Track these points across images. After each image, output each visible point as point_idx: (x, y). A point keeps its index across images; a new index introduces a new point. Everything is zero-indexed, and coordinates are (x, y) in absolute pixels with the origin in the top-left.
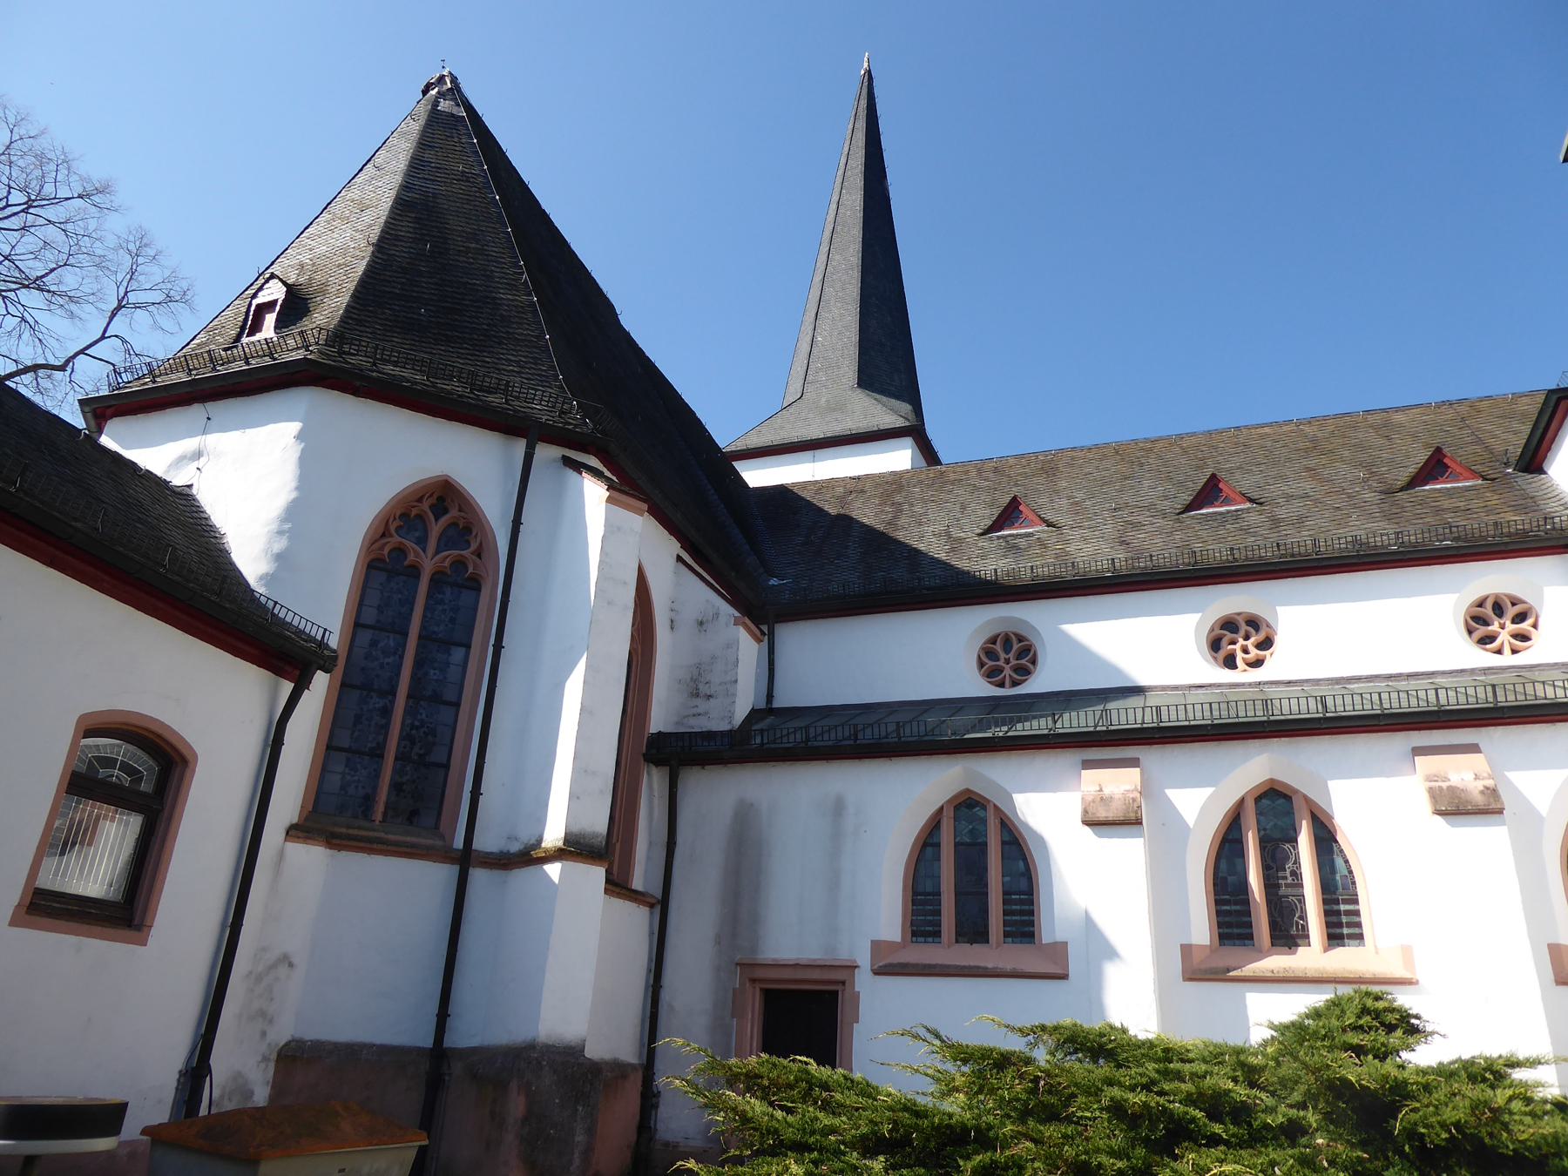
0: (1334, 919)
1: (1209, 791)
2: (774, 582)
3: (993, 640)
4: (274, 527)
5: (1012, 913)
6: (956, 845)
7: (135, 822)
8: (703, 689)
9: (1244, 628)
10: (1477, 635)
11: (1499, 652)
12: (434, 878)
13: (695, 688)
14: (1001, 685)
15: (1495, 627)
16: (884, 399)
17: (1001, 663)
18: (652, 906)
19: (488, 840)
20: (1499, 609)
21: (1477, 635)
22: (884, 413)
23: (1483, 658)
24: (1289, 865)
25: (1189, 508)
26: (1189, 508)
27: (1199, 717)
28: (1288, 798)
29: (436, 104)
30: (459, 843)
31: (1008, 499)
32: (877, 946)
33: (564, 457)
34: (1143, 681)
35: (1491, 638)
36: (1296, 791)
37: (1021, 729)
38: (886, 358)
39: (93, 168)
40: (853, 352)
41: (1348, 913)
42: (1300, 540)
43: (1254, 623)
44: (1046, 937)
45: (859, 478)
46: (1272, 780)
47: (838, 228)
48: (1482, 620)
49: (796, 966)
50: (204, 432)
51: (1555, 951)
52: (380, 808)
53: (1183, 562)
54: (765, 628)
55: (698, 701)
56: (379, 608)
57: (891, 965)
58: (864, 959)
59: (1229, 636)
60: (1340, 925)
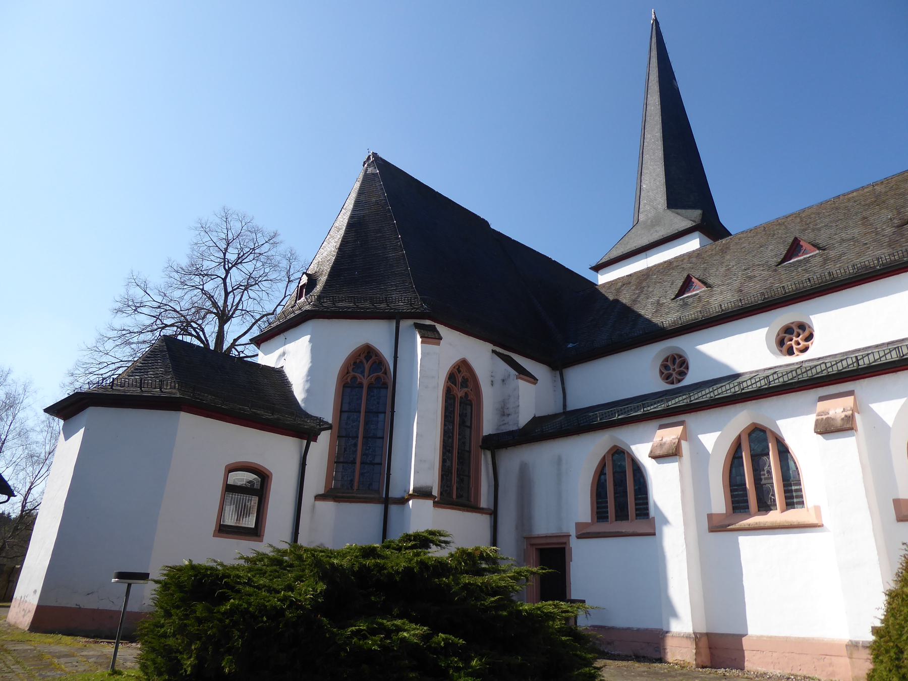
0: (788, 494)
1: (718, 434)
2: (570, 345)
3: (666, 360)
6: (614, 473)
7: (257, 499)
8: (506, 412)
9: (796, 330)
12: (378, 509)
13: (503, 411)
14: (673, 383)
16: (683, 211)
18: (491, 514)
19: (395, 493)
22: (680, 221)
24: (766, 468)
29: (367, 170)
31: (791, 240)
33: (415, 324)
34: (740, 369)
37: (651, 409)
38: (687, 183)
39: (269, 227)
40: (663, 189)
41: (796, 491)
42: (838, 269)
45: (630, 275)
47: (648, 119)
49: (546, 537)
51: (897, 503)
54: (558, 373)
56: (349, 403)
57: (584, 534)
58: (573, 533)
59: (788, 336)
60: (792, 497)
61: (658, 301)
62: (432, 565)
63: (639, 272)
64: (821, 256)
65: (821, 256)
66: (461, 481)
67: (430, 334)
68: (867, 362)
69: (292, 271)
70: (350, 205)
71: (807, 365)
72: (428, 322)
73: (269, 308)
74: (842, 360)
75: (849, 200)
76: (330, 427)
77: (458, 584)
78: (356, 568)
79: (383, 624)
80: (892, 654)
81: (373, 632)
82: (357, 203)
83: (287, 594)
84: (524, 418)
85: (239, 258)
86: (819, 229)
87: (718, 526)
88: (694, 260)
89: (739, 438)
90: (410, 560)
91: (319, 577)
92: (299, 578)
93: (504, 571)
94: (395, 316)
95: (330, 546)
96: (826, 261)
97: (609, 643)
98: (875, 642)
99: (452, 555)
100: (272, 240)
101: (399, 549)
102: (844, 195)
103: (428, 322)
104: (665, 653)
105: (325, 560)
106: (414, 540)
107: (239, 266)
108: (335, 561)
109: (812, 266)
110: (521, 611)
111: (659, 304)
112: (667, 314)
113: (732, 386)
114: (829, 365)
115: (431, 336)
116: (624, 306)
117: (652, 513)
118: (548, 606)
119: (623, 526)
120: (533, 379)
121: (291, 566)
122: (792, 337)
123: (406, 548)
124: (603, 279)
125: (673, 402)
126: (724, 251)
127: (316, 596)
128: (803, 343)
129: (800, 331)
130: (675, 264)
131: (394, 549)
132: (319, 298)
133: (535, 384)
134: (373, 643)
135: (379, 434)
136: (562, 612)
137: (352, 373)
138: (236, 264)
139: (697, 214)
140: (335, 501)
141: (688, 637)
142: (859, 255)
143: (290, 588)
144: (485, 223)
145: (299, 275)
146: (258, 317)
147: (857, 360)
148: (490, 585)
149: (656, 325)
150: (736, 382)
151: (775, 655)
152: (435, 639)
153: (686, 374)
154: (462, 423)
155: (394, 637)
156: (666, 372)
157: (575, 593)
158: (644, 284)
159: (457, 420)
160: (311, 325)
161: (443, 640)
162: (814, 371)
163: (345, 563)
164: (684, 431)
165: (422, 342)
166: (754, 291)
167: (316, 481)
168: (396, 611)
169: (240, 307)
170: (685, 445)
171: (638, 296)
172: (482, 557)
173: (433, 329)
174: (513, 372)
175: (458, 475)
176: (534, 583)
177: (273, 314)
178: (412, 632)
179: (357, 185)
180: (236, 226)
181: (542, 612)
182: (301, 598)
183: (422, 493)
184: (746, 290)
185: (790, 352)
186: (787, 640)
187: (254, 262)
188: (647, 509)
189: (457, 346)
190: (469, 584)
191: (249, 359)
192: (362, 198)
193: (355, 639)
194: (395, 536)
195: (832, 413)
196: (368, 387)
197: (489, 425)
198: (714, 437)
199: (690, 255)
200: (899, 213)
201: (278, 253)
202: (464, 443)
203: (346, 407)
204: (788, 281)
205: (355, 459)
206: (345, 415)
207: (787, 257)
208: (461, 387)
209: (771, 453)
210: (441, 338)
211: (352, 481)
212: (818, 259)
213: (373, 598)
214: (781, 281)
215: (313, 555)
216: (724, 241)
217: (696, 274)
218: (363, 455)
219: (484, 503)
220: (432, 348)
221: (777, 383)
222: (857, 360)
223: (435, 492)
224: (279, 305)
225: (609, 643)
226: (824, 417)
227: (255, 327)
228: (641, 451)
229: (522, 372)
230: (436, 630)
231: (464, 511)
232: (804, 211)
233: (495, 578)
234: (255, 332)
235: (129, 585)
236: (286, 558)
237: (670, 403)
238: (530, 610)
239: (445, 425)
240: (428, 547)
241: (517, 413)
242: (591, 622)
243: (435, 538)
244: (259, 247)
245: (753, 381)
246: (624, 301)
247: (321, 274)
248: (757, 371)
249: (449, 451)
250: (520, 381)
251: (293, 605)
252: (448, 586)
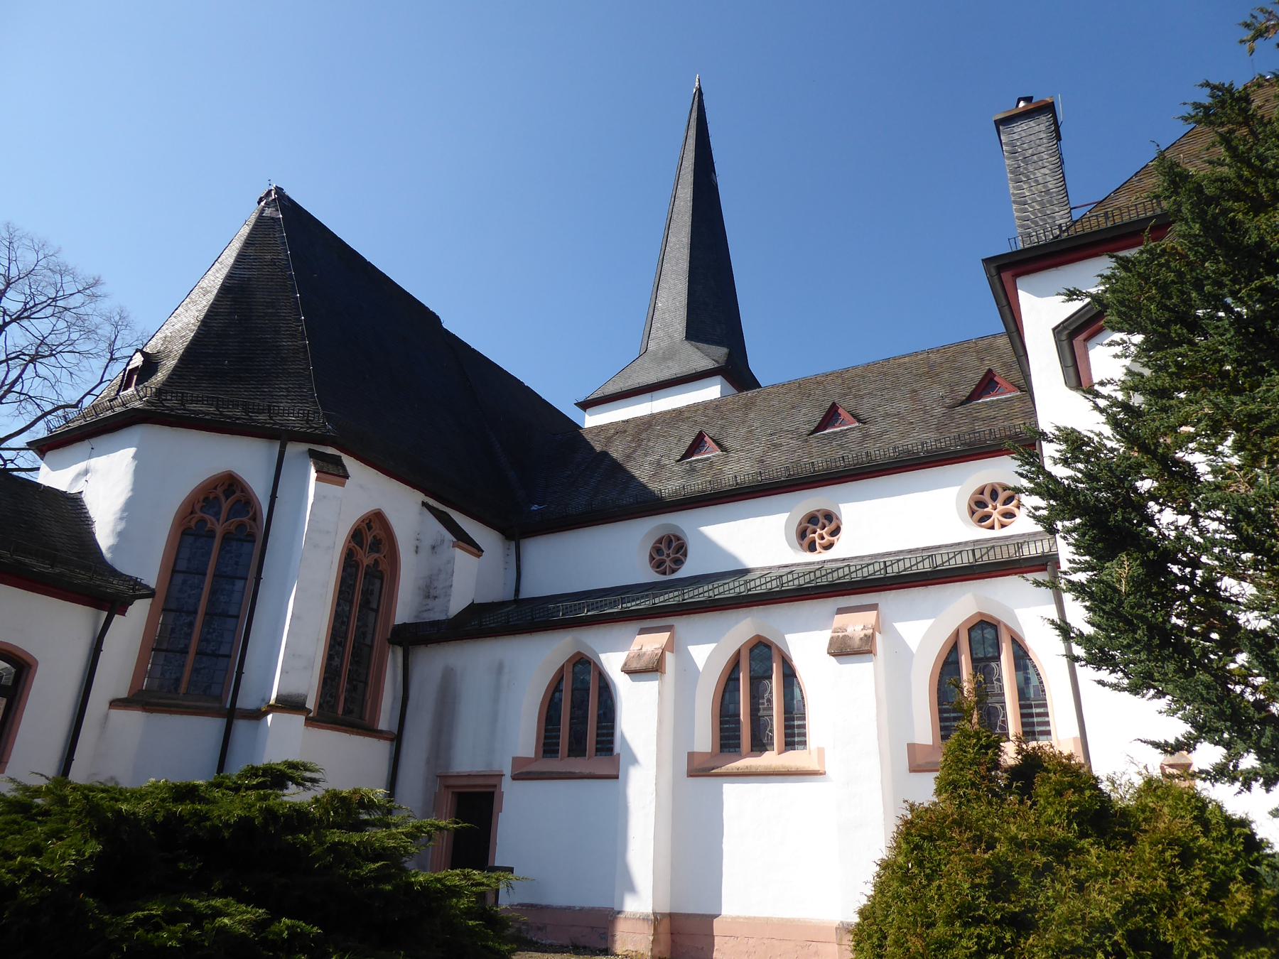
1: (713, 646)
2: (535, 507)
3: (660, 541)
4: (118, 515)
5: (947, 719)
8: (433, 593)
9: (822, 520)
10: (977, 516)
11: (992, 527)
13: (429, 591)
14: (664, 573)
15: (989, 509)
16: (706, 346)
18: (392, 740)
20: (994, 495)
22: (699, 358)
23: (982, 533)
24: (766, 695)
25: (817, 429)
26: (817, 429)
29: (263, 211)
31: (828, 405)
34: (750, 564)
35: (988, 516)
36: (999, 622)
37: (632, 606)
38: (713, 310)
39: (87, 270)
42: (878, 450)
46: (980, 614)
47: (674, 216)
48: (981, 504)
50: (90, 458)
52: (184, 685)
54: (513, 545)
55: (429, 601)
58: (508, 771)
59: (811, 527)
60: (793, 735)
61: (659, 461)
62: (283, 815)
63: (640, 418)
64: (861, 430)
65: (861, 430)
66: (353, 689)
67: (331, 468)
68: (896, 570)
69: (118, 344)
70: (229, 258)
71: (827, 566)
72: (331, 451)
73: (71, 396)
74: (868, 565)
75: (899, 365)
76: (151, 594)
77: (322, 843)
78: (159, 818)
79: (191, 905)
80: (875, 940)
81: (172, 919)
82: (241, 258)
83: (27, 860)
84: (457, 603)
85: (26, 310)
86: (862, 397)
87: (700, 768)
88: (710, 412)
89: (738, 654)
90: (251, 806)
91: (92, 831)
92: (57, 835)
93: (396, 826)
94: (280, 435)
95: (126, 782)
96: (866, 436)
97: (539, 929)
98: (858, 924)
99: (317, 800)
100: (90, 289)
101: (237, 789)
102: (894, 359)
103: (331, 451)
104: (613, 942)
105: (106, 804)
106: (263, 776)
107: (25, 323)
108: (124, 807)
109: (848, 441)
110: (412, 884)
111: (659, 465)
112: (669, 479)
113: (737, 584)
114: (853, 569)
115: (332, 471)
116: (614, 461)
117: (617, 748)
118: (454, 877)
119: (577, 765)
120: (476, 549)
121: (46, 813)
123: (248, 788)
124: (592, 420)
125: (662, 599)
126: (748, 406)
127: (80, 864)
128: (827, 538)
129: (827, 523)
130: (686, 414)
131: (228, 788)
132: (159, 392)
133: (479, 556)
134: (168, 937)
135: (233, 611)
136: (472, 885)
137: (199, 514)
138: (19, 318)
139: (721, 352)
140: (145, 710)
141: (645, 919)
142: (903, 435)
143: (37, 851)
144: (435, 319)
145: (130, 352)
146: (48, 408)
147: (886, 567)
148: (372, 845)
149: (652, 492)
150: (742, 581)
151: (751, 941)
152: (275, 927)
153: (683, 563)
154: (365, 604)
155: (208, 926)
156: (658, 558)
157: (500, 858)
158: (644, 436)
159: (358, 597)
160: (139, 432)
161: (288, 928)
162: (835, 575)
163: (141, 809)
164: (671, 639)
165: (318, 479)
166: (779, 464)
167: (117, 671)
168: (217, 885)
169: (17, 388)
170: (670, 658)
171: (634, 451)
172: (361, 804)
173: (337, 462)
174: (449, 536)
175: (350, 681)
176: (443, 844)
177: (76, 406)
178: (237, 917)
179: (246, 230)
180: (27, 258)
181: (443, 885)
182: (54, 867)
183: (289, 704)
184: (769, 461)
185: (812, 548)
186: (767, 923)
187: (54, 320)
188: (612, 742)
189: (369, 490)
190: (340, 843)
191: (23, 475)
192: (251, 251)
193: (140, 931)
194: (236, 767)
195: (850, 631)
196: (221, 541)
197: (404, 610)
198: (708, 650)
199: (705, 405)
200: (952, 391)
201: (95, 312)
202: (364, 634)
203: (183, 565)
204: (819, 456)
205: (187, 646)
206: (179, 578)
207: (822, 426)
208: (369, 550)
209: (1003, 657)
210: (347, 477)
211: (178, 681)
212: (856, 434)
213: (181, 865)
214: (810, 455)
215: (86, 797)
216: (750, 393)
217: (711, 431)
218: (201, 641)
219: (383, 724)
220: (332, 489)
221: (791, 586)
222: (886, 567)
223: (311, 704)
224: (89, 393)
225: (539, 929)
226: (841, 634)
227: (41, 424)
228: (612, 663)
229: (464, 539)
230: (276, 916)
231: (352, 733)
232: (847, 370)
233: (379, 835)
234: (40, 431)
236: (39, 801)
237: (657, 600)
238: (426, 881)
239: (338, 605)
240: (283, 786)
241: (448, 595)
242: (516, 899)
243: (296, 774)
244: (65, 297)
245: (763, 581)
246: (615, 455)
247: (168, 356)
248: (770, 568)
249: (340, 644)
250: (458, 551)
251: (36, 878)
252: (307, 847)
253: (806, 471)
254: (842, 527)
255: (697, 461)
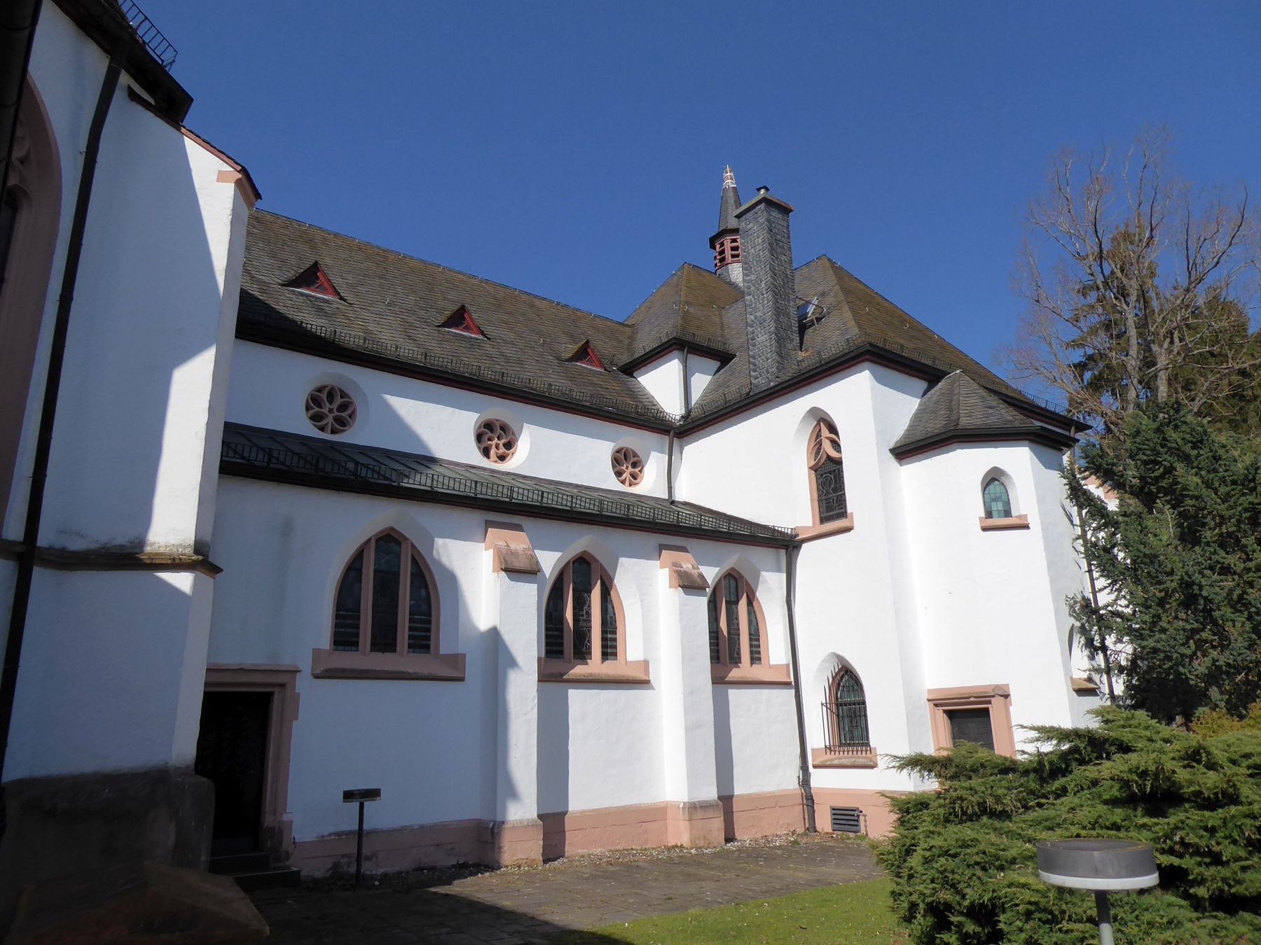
3: (320, 390)
14: (322, 429)
15: (624, 468)
17: (325, 411)
21: (311, 412)
23: (477, 459)
25: (443, 325)
27: (564, 503)
28: (588, 564)
30: (14, 530)
32: (317, 653)
33: (129, 87)
36: (742, 577)
43: (504, 428)
44: (445, 648)
53: (419, 360)
57: (336, 670)
58: (306, 665)
122: (494, 436)
128: (502, 450)
235: (729, 839)
253: (488, 375)
254: (472, 438)
255: (302, 294)
